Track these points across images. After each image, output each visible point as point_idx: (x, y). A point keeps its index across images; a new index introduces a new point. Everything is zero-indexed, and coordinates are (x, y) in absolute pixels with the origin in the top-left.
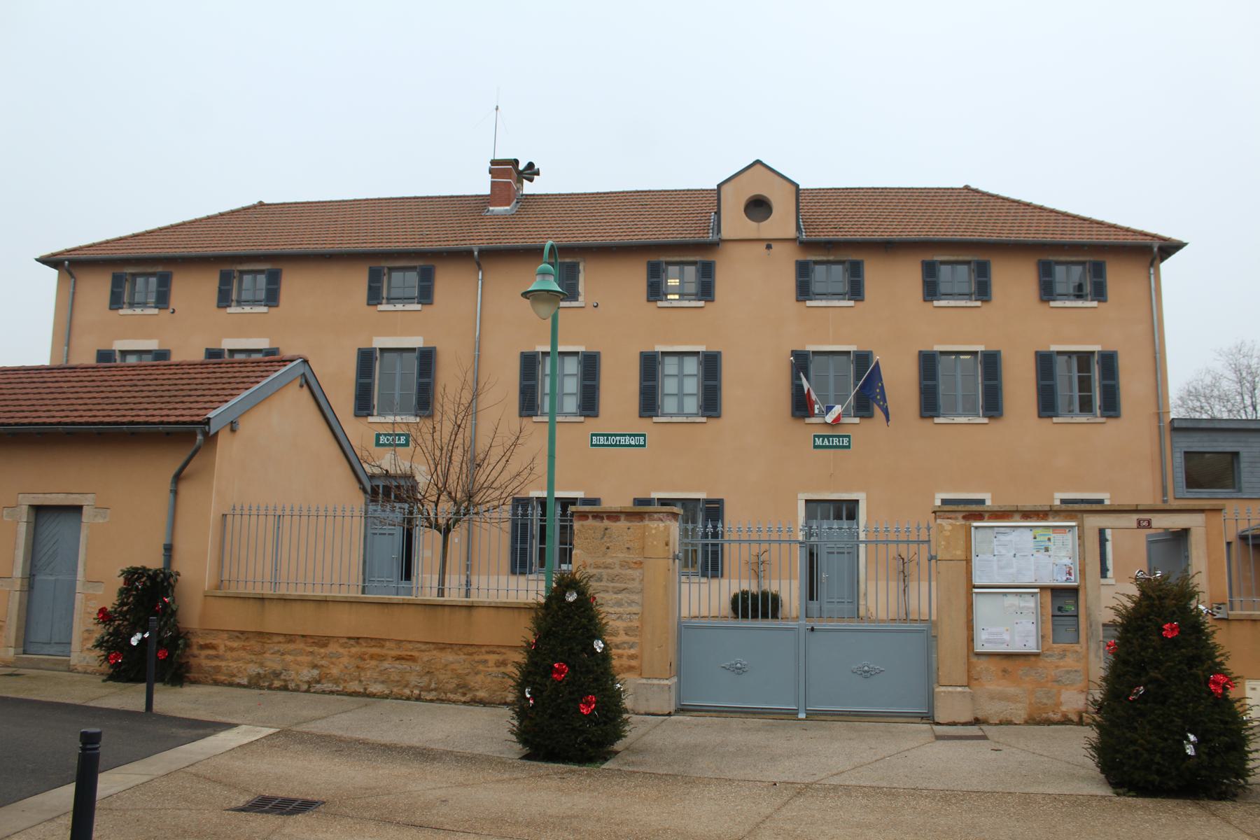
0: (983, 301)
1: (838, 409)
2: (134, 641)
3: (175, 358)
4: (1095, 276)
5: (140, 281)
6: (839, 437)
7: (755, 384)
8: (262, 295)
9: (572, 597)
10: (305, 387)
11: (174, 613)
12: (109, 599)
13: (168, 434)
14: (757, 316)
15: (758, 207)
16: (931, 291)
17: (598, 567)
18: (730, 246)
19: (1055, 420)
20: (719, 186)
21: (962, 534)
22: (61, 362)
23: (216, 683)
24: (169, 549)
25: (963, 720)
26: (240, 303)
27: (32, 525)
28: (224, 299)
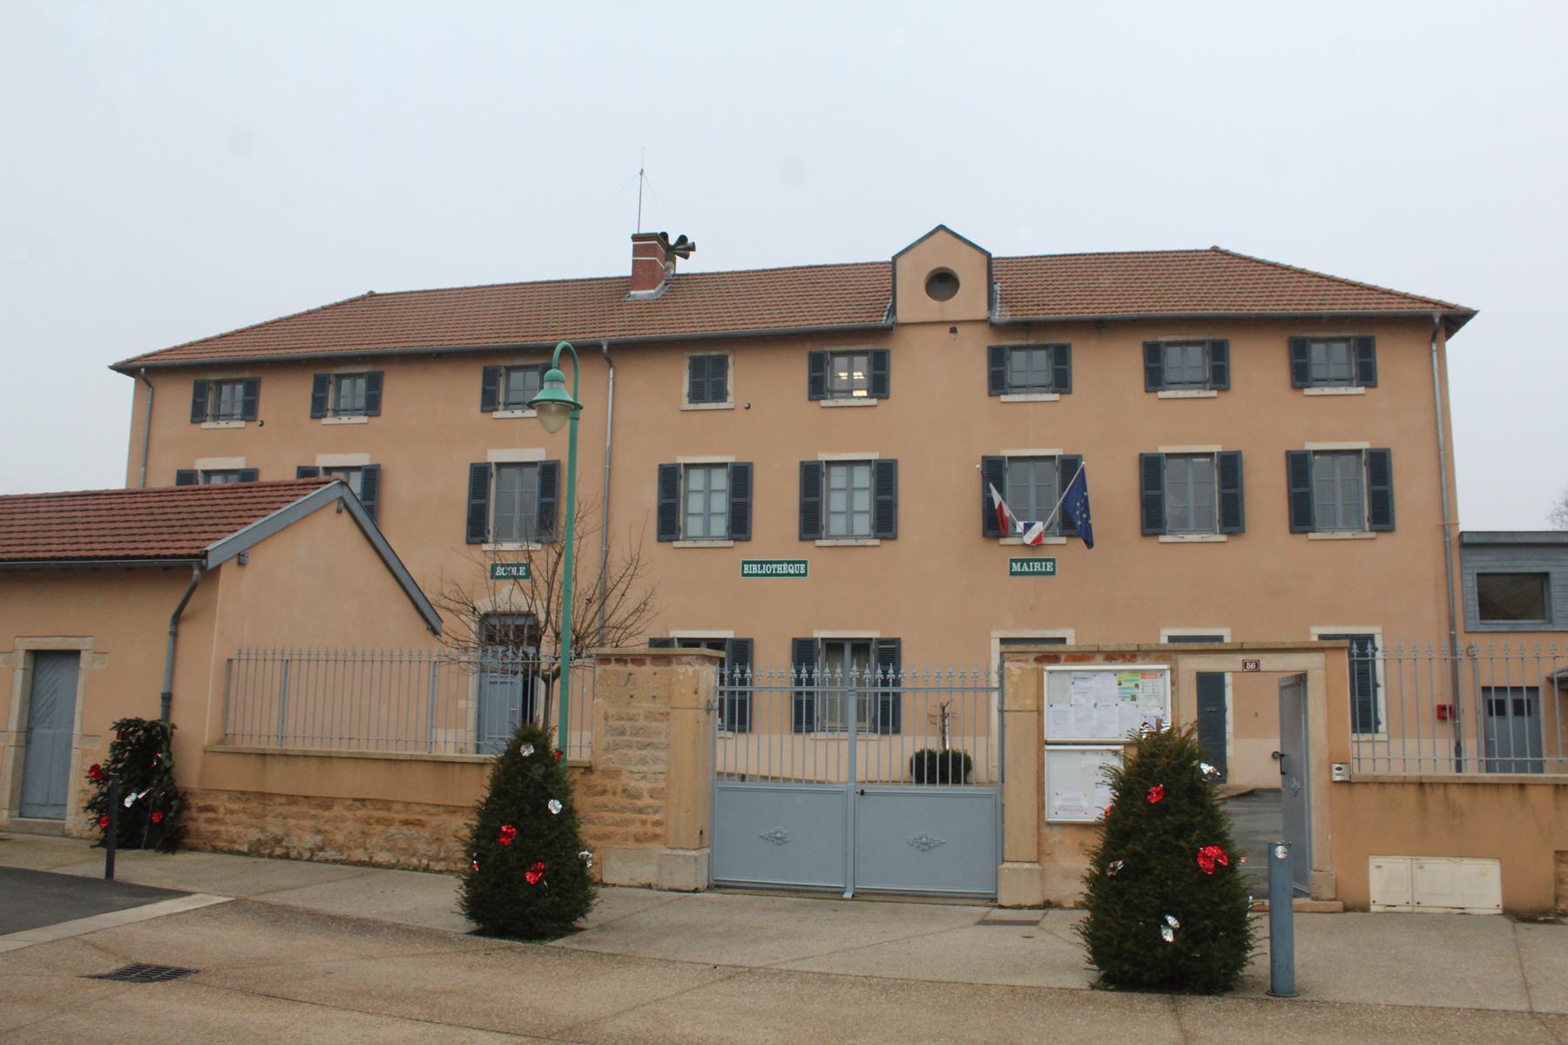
0: (1219, 390)
1: (1039, 527)
2: (128, 803)
3: (264, 478)
4: (1361, 355)
5: (226, 389)
6: (1040, 561)
7: (939, 498)
8: (361, 402)
9: (527, 751)
10: (345, 513)
11: (168, 770)
12: (101, 753)
13: (165, 569)
14: (941, 414)
15: (942, 282)
16: (1155, 379)
17: (621, 719)
18: (907, 331)
19: (1311, 536)
20: (895, 258)
21: (1034, 679)
22: (137, 486)
23: (215, 850)
24: (167, 699)
25: (1030, 902)
26: (337, 412)
27: (30, 674)
28: (319, 408)
